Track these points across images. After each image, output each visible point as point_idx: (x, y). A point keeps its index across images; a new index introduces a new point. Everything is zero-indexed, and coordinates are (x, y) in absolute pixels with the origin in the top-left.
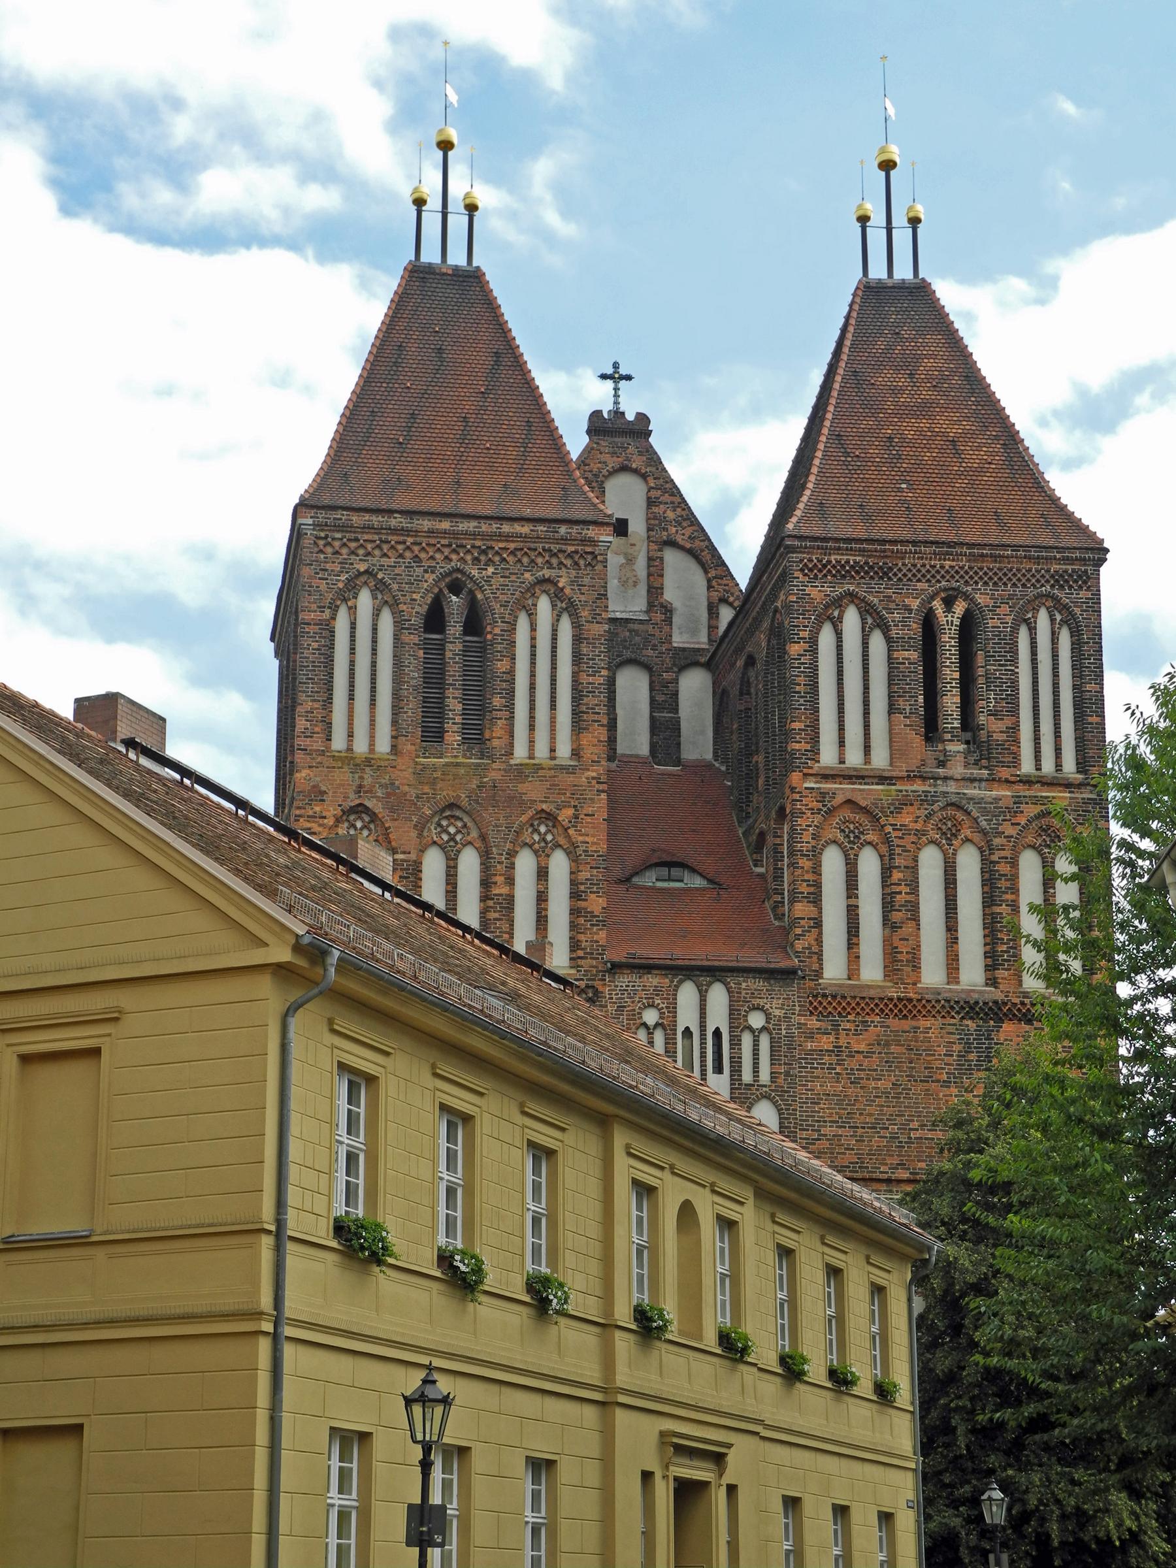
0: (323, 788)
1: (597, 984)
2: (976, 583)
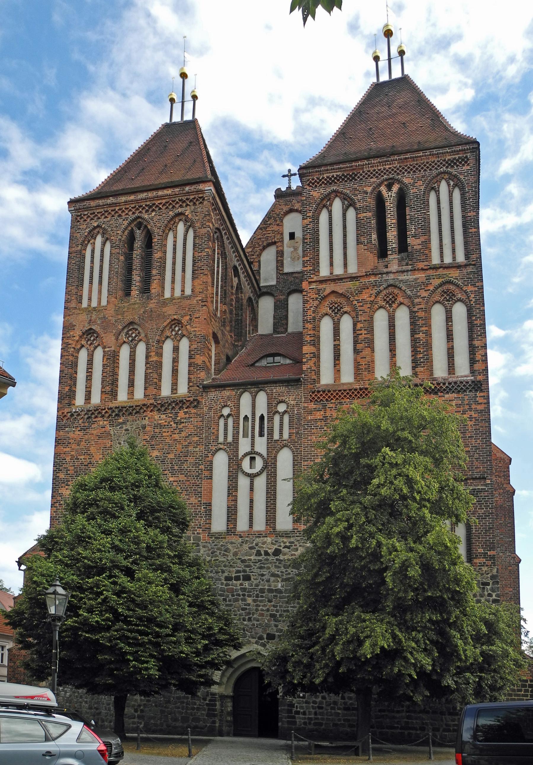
0: (74, 324)
1: (199, 398)
2: (404, 173)
